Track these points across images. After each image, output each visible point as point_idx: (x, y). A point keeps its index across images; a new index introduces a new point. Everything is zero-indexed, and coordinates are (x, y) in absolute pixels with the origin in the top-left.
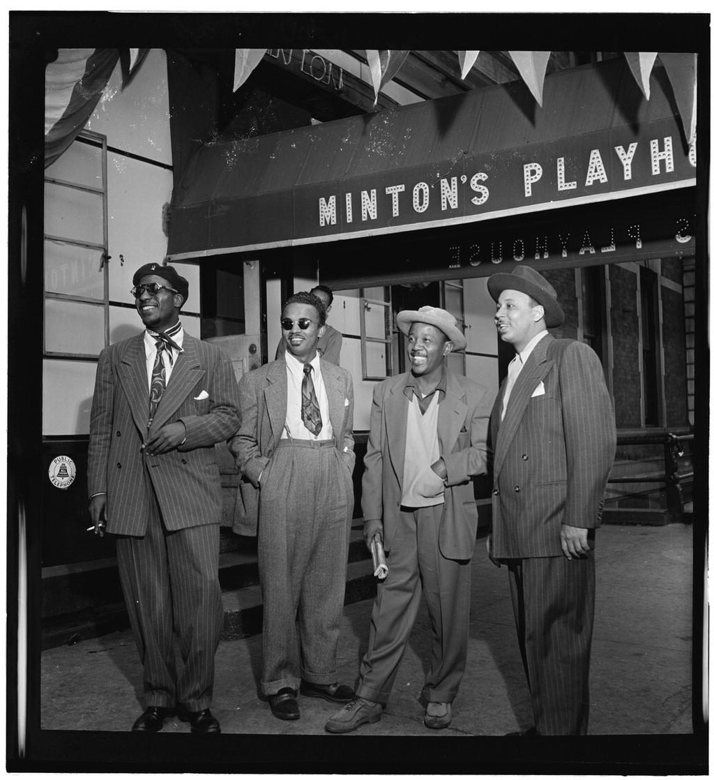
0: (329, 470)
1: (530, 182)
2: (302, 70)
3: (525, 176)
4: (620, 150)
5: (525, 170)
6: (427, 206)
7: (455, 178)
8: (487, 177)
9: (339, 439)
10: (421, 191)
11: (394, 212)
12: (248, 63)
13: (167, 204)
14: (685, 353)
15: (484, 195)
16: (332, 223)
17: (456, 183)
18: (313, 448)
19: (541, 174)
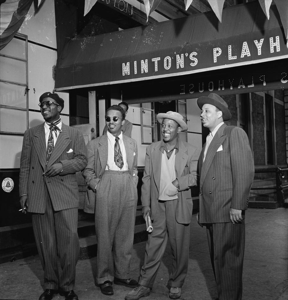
0: (127, 184)
1: (216, 56)
2: (115, 6)
3: (214, 53)
4: (256, 42)
5: (214, 51)
6: (170, 67)
7: (183, 54)
8: (197, 54)
10: (168, 60)
11: (156, 69)
12: (90, 3)
13: (54, 66)
14: (285, 132)
15: (195, 62)
16: (128, 74)
17: (183, 57)
18: (119, 174)
19: (221, 52)
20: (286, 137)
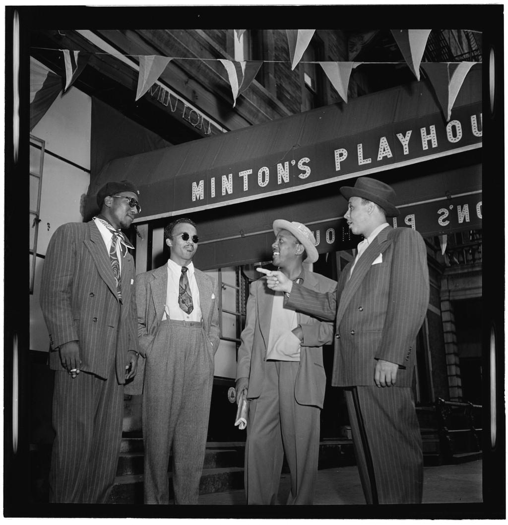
0: (196, 344)
1: (339, 161)
2: (183, 117)
3: (336, 157)
4: (400, 136)
5: (336, 153)
6: (267, 182)
7: (287, 163)
8: (309, 160)
9: (206, 322)
10: (264, 173)
11: (245, 188)
12: (147, 83)
13: (84, 194)
14: (445, 357)
15: (307, 172)
16: (201, 199)
17: (288, 166)
18: (185, 327)
19: (347, 155)
20: (447, 376)
